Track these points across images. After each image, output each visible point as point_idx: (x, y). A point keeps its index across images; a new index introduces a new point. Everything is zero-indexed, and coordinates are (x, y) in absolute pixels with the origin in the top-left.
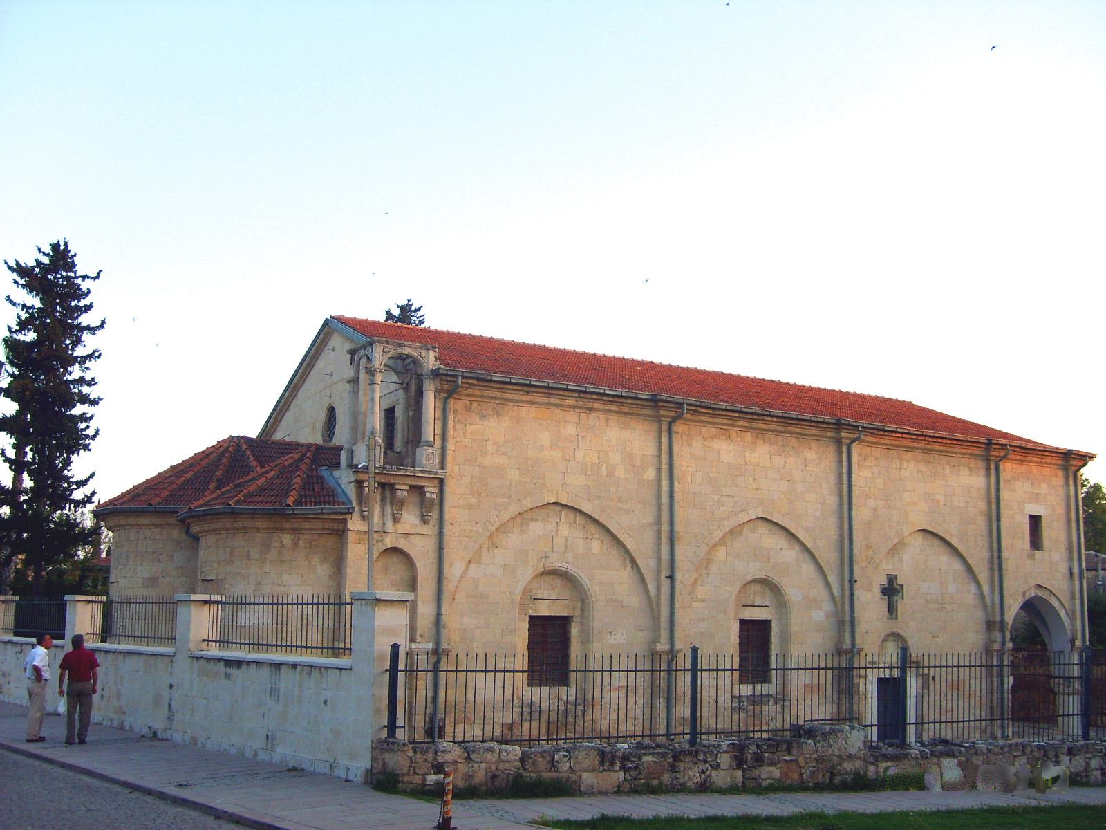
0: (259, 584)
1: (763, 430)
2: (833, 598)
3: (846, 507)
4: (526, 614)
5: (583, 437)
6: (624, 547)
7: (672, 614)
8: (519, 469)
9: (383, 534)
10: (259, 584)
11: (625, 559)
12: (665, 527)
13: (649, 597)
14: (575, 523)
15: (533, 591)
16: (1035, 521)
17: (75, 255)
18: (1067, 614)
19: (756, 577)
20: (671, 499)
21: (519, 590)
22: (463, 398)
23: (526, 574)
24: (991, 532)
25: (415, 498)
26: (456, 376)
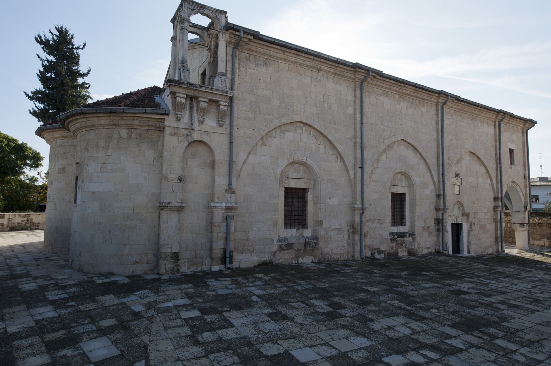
0: (104, 163)
1: (404, 94)
2: (434, 183)
3: (440, 137)
4: (283, 187)
5: (315, 85)
6: (337, 150)
7: (362, 188)
8: (279, 99)
9: (191, 131)
10: (104, 163)
11: (337, 157)
12: (359, 140)
13: (350, 179)
14: (311, 134)
15: (287, 173)
16: (511, 151)
18: (523, 194)
19: (400, 170)
20: (361, 125)
21: (279, 172)
22: (245, 51)
23: (283, 163)
24: (496, 154)
25: (213, 109)
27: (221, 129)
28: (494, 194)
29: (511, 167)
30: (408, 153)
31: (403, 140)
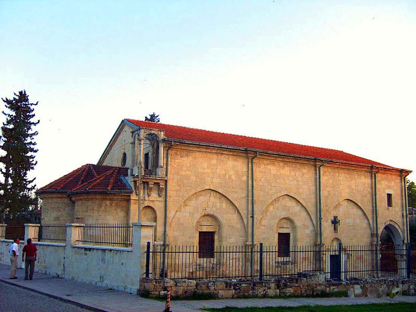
6: (235, 205)
7: (253, 231)
16: (389, 196)
17: (28, 96)
23: (198, 216)
26: (172, 141)
27: (160, 198)
28: (371, 232)
29: (388, 209)
30: (292, 204)
31: (286, 195)
